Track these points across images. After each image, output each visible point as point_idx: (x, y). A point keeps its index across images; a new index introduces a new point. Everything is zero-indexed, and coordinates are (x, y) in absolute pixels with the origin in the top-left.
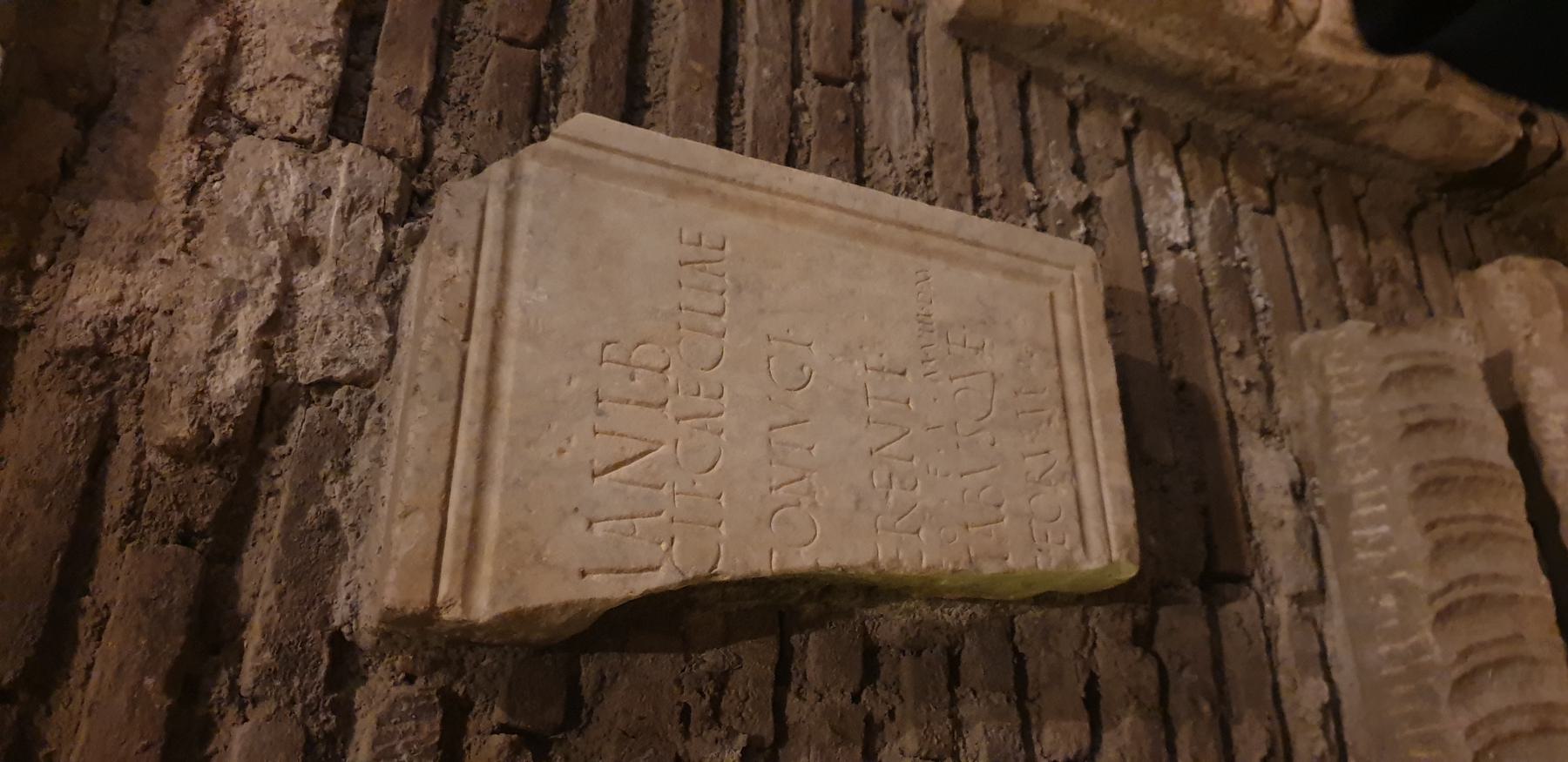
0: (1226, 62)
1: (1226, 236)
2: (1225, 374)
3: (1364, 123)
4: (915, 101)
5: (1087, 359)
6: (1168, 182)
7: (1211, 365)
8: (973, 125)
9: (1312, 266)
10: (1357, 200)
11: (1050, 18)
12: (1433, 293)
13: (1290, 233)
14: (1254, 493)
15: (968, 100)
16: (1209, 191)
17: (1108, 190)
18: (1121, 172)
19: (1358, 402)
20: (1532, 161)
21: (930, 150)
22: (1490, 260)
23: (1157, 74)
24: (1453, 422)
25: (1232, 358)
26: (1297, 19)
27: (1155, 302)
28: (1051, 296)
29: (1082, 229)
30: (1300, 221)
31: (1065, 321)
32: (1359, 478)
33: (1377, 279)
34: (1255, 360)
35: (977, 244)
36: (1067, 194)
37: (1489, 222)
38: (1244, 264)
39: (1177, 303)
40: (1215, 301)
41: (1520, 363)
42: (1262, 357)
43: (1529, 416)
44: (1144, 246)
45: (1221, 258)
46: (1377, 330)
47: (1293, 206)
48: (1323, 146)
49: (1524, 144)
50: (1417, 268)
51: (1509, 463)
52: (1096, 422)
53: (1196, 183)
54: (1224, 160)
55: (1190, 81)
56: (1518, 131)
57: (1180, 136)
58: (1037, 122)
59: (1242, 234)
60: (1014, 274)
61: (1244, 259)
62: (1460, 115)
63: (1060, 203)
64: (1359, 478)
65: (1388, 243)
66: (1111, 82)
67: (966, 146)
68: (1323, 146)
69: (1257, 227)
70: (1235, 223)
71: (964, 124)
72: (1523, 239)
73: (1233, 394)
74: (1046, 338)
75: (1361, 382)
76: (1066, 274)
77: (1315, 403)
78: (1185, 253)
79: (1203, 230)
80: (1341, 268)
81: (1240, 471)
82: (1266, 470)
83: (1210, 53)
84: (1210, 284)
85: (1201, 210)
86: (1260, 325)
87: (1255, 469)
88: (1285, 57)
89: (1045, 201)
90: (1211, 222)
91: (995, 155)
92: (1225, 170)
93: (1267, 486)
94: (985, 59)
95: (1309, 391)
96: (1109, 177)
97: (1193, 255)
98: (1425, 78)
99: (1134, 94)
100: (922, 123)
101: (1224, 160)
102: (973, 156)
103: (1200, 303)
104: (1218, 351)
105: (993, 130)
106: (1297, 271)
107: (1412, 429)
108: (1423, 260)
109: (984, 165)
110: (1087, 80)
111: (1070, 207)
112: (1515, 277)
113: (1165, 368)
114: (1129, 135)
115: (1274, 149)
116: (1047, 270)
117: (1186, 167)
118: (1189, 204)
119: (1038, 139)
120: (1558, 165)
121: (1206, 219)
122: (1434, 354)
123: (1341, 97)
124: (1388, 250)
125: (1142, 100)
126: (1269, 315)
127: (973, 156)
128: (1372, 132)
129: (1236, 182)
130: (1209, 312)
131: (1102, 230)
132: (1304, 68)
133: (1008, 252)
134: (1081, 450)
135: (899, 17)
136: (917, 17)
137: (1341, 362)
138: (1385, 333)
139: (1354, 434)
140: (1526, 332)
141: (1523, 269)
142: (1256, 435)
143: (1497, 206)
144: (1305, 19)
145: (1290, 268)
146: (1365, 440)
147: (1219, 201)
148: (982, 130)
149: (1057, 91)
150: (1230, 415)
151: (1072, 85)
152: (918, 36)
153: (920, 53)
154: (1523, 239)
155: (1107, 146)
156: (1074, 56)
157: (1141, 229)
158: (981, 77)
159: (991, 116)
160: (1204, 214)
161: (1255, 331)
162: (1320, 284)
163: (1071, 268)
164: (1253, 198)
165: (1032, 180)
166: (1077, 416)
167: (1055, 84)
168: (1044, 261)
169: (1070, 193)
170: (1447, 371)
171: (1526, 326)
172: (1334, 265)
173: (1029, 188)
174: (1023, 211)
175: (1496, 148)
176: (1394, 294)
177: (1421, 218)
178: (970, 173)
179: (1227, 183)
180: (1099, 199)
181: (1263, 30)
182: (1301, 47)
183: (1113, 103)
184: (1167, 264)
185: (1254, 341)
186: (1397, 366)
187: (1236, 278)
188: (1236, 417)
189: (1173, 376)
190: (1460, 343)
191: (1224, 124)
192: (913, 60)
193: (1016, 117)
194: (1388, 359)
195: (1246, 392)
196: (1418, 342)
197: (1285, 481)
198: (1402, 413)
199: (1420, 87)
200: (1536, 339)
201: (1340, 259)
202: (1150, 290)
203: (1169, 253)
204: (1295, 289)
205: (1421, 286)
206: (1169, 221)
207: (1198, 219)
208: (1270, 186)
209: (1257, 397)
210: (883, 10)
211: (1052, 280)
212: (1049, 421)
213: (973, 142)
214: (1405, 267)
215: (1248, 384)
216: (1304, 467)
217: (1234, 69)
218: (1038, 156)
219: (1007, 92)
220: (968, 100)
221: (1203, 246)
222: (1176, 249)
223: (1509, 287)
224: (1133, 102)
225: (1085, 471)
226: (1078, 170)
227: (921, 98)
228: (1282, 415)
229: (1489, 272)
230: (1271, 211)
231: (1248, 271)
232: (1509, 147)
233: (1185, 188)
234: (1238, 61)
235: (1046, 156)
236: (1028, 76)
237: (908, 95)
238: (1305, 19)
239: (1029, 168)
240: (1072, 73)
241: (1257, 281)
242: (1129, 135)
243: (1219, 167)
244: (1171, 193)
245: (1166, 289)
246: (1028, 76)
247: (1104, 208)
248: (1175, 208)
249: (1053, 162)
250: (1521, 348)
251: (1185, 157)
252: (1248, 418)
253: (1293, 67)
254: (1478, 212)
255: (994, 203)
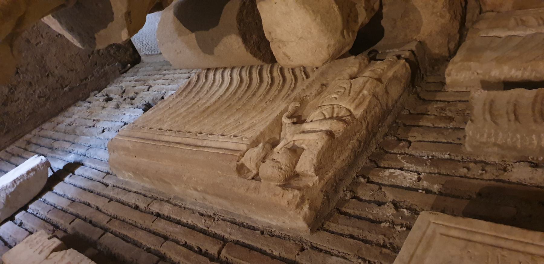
0: (354, 141)
1: (418, 160)
2: (476, 177)
3: (387, 105)
4: (338, 256)
5: (474, 230)
6: (391, 174)
7: (471, 181)
8: (352, 237)
9: (435, 134)
10: (410, 113)
11: (322, 195)
12: (451, 99)
13: (419, 138)
14: (532, 182)
15: (342, 235)
16: (397, 160)
17: (390, 196)
18: (383, 189)
19: (501, 134)
20: (412, 59)
21: (359, 258)
22: (445, 78)
23: (351, 165)
24: (515, 105)
25: (470, 173)
26: (348, 116)
27: (440, 194)
28: (441, 234)
29: (405, 210)
30: (415, 134)
31: (453, 233)
32: (535, 142)
33: (444, 115)
34: (471, 165)
35: (412, 257)
36: (389, 211)
37: (427, 76)
38: (430, 157)
39: (443, 185)
40: (443, 171)
41: (487, 78)
42: (471, 162)
43: (510, 80)
44: (417, 190)
45: (426, 164)
46: (472, 121)
47: (410, 134)
48: (390, 119)
49: (407, 60)
50: (440, 101)
51: (535, 91)
52: (505, 236)
53: (394, 164)
54: (386, 152)
55: (356, 155)
56: (403, 61)
57: (374, 164)
58: (357, 213)
59: (417, 154)
60: (429, 246)
61: (428, 157)
62: (393, 76)
63: (392, 215)
64: (535, 142)
65: (430, 108)
66: (349, 181)
67: (360, 242)
68: (390, 119)
69: (415, 149)
70: (413, 155)
71: (352, 240)
72: (436, 68)
73: (486, 176)
74: (462, 243)
75: (493, 131)
76: (432, 226)
77: (496, 149)
78: (421, 176)
79: (413, 167)
80: (436, 125)
81: (521, 184)
82: (521, 174)
83: (350, 146)
84: (436, 172)
85: (405, 165)
86: (456, 158)
87: (521, 178)
88: (359, 123)
89: (391, 221)
90: (411, 163)
91: (367, 233)
92: (390, 153)
93: (531, 176)
94: (327, 223)
95: (490, 150)
96: (385, 194)
97: (423, 174)
98: (379, 83)
99: (355, 175)
100: (347, 257)
101: (386, 152)
102: (365, 241)
103: (444, 177)
104: (466, 177)
105: (356, 230)
106: (435, 140)
107: (517, 119)
108: (437, 99)
109: (369, 238)
110: (345, 190)
111: (395, 212)
112: (453, 73)
113: (470, 198)
114: (369, 182)
115: (386, 135)
116: (429, 232)
117: (386, 166)
118: (401, 169)
119: (364, 215)
120: (415, 52)
121: (409, 165)
122: (485, 104)
123: (377, 109)
124: (432, 109)
125: (357, 173)
126: (452, 154)
127: (365, 241)
128: (390, 103)
129: (395, 151)
130: (448, 175)
131: (406, 203)
132: (364, 117)
133: (418, 245)
134: (519, 247)
135: (303, 249)
136: (304, 242)
137: (482, 135)
138: (473, 118)
139: (515, 139)
140: (476, 74)
141: (451, 70)
142: (506, 174)
143: (422, 72)
144: (348, 114)
145: (434, 142)
146: (518, 136)
147: (402, 158)
148: (355, 234)
149: (347, 201)
150: (494, 180)
151: (346, 195)
152: (311, 245)
153: (318, 246)
154: (436, 68)
155: (373, 191)
156: (336, 192)
157: (408, 189)
158: (333, 227)
159: (350, 229)
160: (406, 165)
161: (459, 161)
162: (443, 134)
163: (430, 222)
164: (403, 147)
165: (380, 222)
166: (502, 243)
167: (343, 201)
168: (424, 233)
169: (389, 210)
170: (492, 103)
171: (473, 73)
172: (435, 127)
173: (383, 225)
174: (393, 230)
175: (407, 68)
176: (450, 111)
177: (421, 95)
178: (372, 245)
179: (396, 154)
180: (393, 200)
181: (348, 127)
182: (357, 117)
183: (355, 183)
184: (425, 184)
185: (464, 163)
186: (488, 117)
187: (435, 162)
188: (496, 178)
189: (475, 196)
190: (479, 96)
191: (373, 148)
192: (321, 251)
193: (353, 220)
194: (485, 119)
195: (486, 172)
196: (478, 109)
197: (530, 169)
198: (509, 121)
199: (381, 85)
200: (479, 71)
201: (433, 125)
202: (435, 193)
203: (420, 182)
204: (444, 143)
205: (449, 102)
206: (408, 178)
207: (408, 168)
208: (400, 140)
209: (488, 168)
210: (298, 255)
211: (434, 232)
212: (503, 256)
213: (359, 239)
214: (440, 105)
215: (483, 170)
216: (523, 160)
217: (358, 140)
218: (371, 217)
219: (342, 219)
220: (342, 235)
221: (420, 169)
222: (419, 179)
223: (457, 75)
224: (357, 176)
225: (532, 250)
226: (380, 204)
227: (336, 253)
228: (497, 162)
229: (448, 80)
230: (410, 143)
231: (433, 156)
232: (407, 65)
233: (395, 169)
234: (355, 138)
235: (372, 214)
236: (338, 209)
237: (334, 258)
238: (348, 114)
239: (376, 222)
240: (341, 194)
241: (437, 154)
242: (369, 182)
243: (389, 155)
244: (396, 174)
245: (436, 188)
246: (338, 209)
247: (397, 200)
248: (402, 174)
249: (375, 212)
250: (481, 77)
251: (382, 165)
252: (497, 174)
253: (363, 121)
254: (423, 78)
255: (386, 240)
